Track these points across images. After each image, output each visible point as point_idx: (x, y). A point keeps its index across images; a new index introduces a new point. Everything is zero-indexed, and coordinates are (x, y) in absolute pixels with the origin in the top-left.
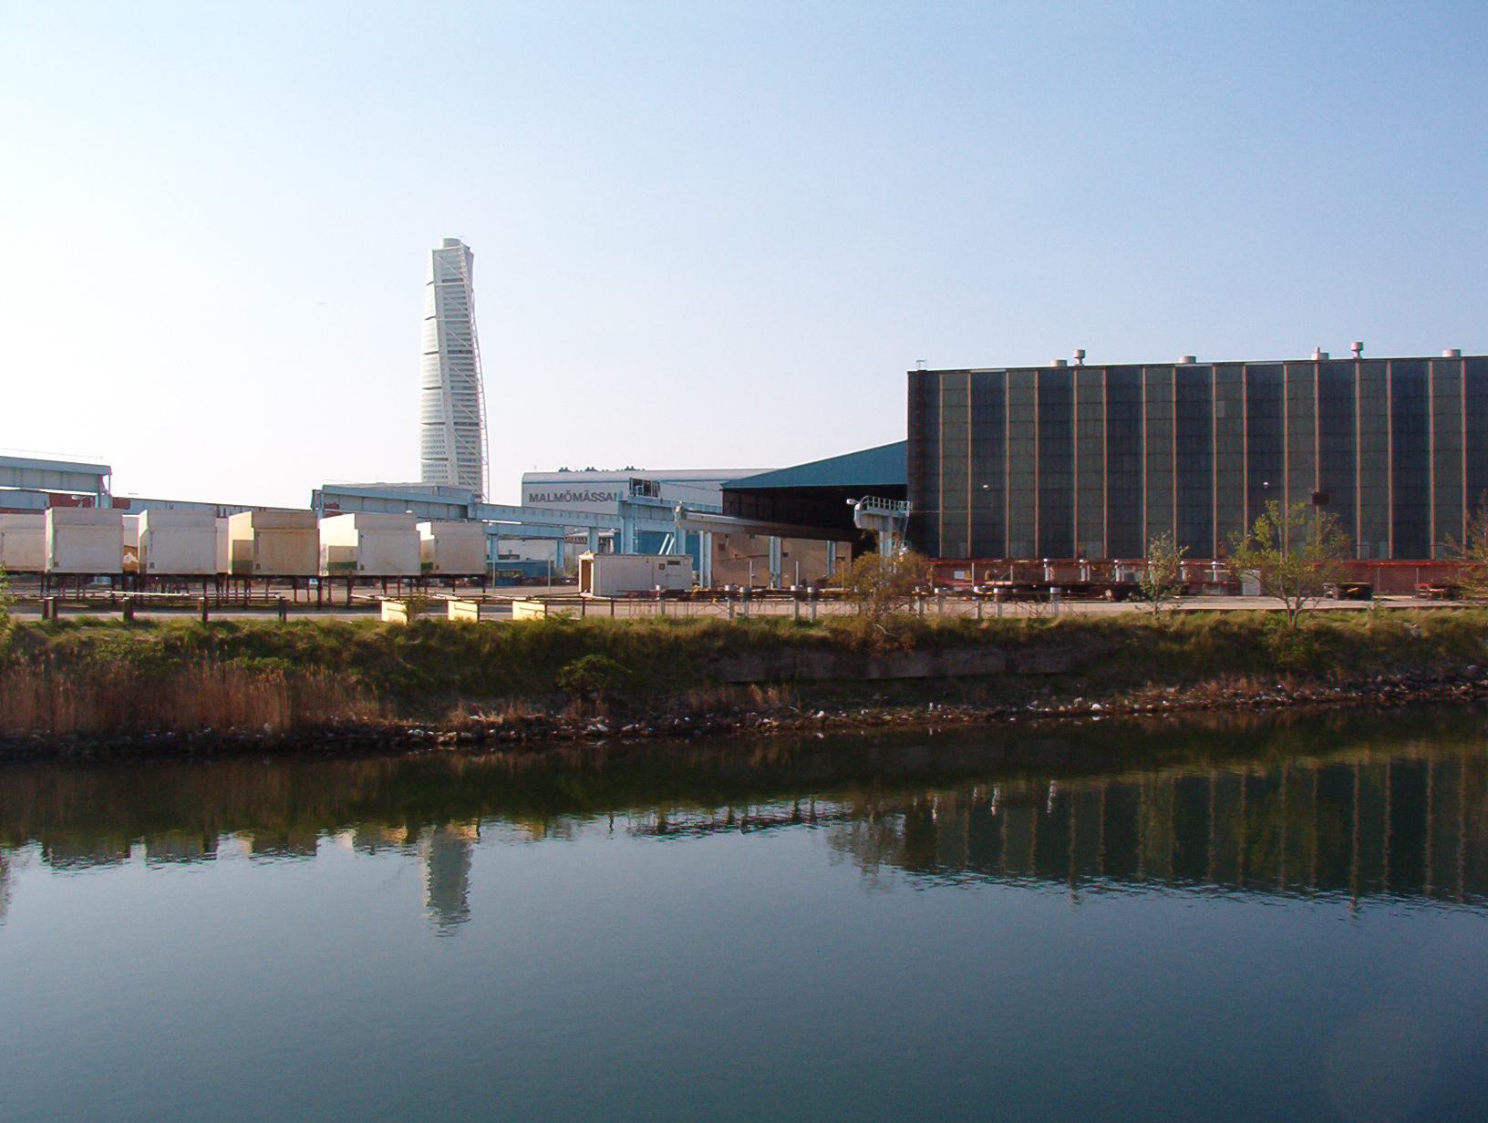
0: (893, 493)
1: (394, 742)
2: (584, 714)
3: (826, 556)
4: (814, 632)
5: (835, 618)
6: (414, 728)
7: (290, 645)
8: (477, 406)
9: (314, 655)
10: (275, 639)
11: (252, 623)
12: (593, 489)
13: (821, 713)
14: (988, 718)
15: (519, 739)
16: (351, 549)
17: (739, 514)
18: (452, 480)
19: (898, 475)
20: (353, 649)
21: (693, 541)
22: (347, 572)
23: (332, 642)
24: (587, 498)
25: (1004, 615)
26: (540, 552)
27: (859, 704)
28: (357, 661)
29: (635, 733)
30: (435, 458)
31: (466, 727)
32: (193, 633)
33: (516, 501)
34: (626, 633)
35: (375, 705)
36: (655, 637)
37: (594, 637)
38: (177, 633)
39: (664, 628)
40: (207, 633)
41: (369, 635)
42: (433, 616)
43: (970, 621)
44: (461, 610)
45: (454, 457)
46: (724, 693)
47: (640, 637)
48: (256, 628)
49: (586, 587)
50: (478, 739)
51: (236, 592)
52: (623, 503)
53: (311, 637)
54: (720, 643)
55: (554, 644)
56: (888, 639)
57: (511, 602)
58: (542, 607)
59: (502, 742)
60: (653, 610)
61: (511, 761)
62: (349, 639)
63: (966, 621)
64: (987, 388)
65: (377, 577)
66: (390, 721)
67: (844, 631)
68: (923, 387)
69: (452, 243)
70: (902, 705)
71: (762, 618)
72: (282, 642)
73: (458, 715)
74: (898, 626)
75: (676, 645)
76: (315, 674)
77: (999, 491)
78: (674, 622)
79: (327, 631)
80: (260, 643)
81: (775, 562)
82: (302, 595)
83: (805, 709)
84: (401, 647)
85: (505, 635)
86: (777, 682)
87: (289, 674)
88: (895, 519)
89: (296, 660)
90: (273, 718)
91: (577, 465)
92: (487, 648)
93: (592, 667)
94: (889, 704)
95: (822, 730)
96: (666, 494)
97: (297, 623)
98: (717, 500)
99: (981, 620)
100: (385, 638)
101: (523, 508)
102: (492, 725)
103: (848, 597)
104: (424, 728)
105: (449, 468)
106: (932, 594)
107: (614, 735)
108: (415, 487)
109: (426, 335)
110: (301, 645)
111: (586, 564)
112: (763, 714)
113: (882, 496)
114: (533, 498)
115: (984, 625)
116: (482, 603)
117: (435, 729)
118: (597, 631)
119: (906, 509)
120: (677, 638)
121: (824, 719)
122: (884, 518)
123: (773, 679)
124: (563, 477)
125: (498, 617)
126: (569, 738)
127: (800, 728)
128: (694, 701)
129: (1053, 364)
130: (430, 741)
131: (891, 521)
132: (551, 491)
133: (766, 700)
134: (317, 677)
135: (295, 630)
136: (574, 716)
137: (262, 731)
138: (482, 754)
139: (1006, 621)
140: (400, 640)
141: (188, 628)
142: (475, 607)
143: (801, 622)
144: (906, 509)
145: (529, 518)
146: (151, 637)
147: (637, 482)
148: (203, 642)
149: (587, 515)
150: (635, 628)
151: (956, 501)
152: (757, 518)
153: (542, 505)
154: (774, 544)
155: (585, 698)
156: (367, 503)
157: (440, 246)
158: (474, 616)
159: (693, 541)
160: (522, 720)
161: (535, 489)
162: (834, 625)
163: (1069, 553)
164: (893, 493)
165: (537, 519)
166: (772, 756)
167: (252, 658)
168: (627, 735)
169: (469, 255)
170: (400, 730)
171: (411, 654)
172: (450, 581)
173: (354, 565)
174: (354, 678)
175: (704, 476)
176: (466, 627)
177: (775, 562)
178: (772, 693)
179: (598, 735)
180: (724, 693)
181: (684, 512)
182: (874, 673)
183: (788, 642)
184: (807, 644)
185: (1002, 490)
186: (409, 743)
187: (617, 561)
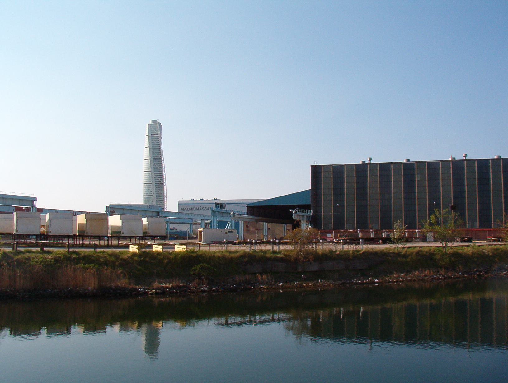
0: (306, 207)
2: (199, 284)
3: (283, 229)
4: (279, 255)
5: (286, 251)
6: (141, 289)
8: (163, 178)
9: (106, 263)
10: (92, 258)
11: (85, 252)
12: (204, 206)
13: (281, 284)
15: (177, 293)
17: (253, 215)
18: (154, 203)
19: (309, 202)
21: (237, 224)
22: (117, 234)
23: (112, 259)
24: (201, 209)
26: (185, 228)
28: (121, 265)
29: (217, 291)
30: (148, 195)
31: (158, 288)
32: (64, 255)
34: (214, 256)
35: (127, 281)
36: (224, 257)
38: (59, 255)
39: (227, 254)
41: (125, 257)
42: (147, 250)
44: (157, 248)
46: (248, 277)
47: (219, 258)
48: (86, 254)
49: (200, 240)
50: (163, 293)
52: (213, 211)
53: (105, 257)
54: (246, 259)
55: (189, 260)
56: (305, 258)
57: (174, 245)
58: (185, 247)
59: (171, 294)
60: (223, 248)
62: (118, 258)
63: (331, 251)
64: (338, 170)
66: (132, 286)
67: (289, 255)
68: (316, 171)
69: (154, 121)
71: (261, 251)
73: (156, 284)
74: (308, 253)
75: (231, 260)
76: (106, 270)
77: (342, 206)
78: (230, 252)
79: (111, 255)
80: (87, 259)
82: (102, 242)
83: (276, 282)
84: (136, 260)
85: (172, 256)
87: (97, 270)
89: (100, 265)
90: (92, 285)
91: (197, 198)
92: (166, 261)
93: (202, 268)
95: (282, 289)
96: (228, 208)
97: (100, 252)
98: (245, 210)
102: (168, 288)
103: (290, 243)
107: (210, 291)
108: (141, 205)
109: (145, 153)
110: (101, 260)
111: (200, 232)
112: (261, 284)
114: (182, 209)
115: (338, 253)
116: (164, 245)
117: (148, 289)
119: (311, 213)
120: (231, 258)
121: (282, 285)
122: (303, 216)
124: (192, 202)
125: (170, 250)
127: (275, 289)
128: (237, 279)
129: (361, 163)
130: (146, 293)
133: (262, 279)
134: (107, 271)
137: (88, 289)
140: (136, 258)
142: (162, 247)
143: (274, 252)
144: (311, 213)
145: (181, 216)
146: (49, 257)
149: (200, 215)
150: (217, 254)
151: (327, 211)
153: (185, 212)
154: (265, 225)
157: (151, 123)
158: (161, 250)
159: (237, 224)
161: (182, 206)
163: (367, 228)
164: (306, 207)
165: (183, 216)
166: (264, 298)
167: (85, 264)
168: (214, 291)
169: (160, 126)
170: (136, 289)
171: (140, 263)
172: (153, 238)
173: (120, 232)
174: (120, 271)
176: (159, 254)
178: (264, 277)
179: (204, 291)
180: (248, 277)
181: (234, 214)
182: (300, 270)
183: (270, 259)
184: (276, 259)
186: (138, 294)
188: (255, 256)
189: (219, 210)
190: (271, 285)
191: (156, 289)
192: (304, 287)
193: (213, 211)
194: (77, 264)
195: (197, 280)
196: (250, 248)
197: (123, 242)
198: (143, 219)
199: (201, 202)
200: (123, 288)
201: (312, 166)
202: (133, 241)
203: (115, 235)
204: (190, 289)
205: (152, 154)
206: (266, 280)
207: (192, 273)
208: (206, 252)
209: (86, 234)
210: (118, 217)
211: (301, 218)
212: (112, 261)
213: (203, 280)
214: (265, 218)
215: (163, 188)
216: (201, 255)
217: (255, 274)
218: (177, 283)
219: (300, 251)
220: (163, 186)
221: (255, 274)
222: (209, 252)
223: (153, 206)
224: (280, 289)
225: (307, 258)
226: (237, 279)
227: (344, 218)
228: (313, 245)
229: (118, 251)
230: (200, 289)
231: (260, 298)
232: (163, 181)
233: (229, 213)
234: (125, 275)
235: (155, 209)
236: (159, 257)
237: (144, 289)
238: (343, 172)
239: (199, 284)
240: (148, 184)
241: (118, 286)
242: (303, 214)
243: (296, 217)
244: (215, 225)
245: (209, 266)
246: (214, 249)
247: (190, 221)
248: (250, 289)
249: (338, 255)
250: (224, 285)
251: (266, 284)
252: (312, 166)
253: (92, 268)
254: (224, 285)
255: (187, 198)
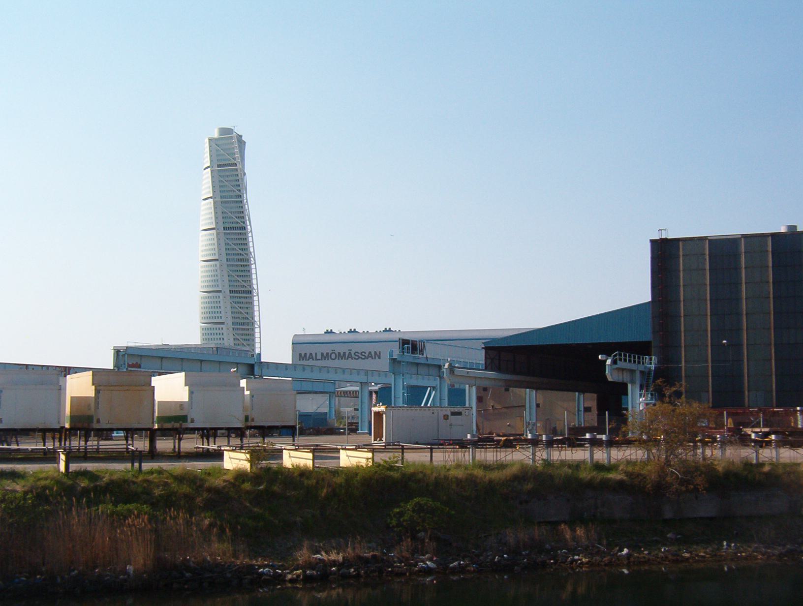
0: (639, 349)
1: (246, 580)
2: (415, 551)
3: (574, 407)
4: (612, 476)
5: (629, 462)
6: (265, 566)
7: (147, 492)
8: (250, 276)
9: (169, 501)
10: (133, 487)
11: (112, 473)
12: (356, 348)
13: (626, 551)
14: (781, 556)
15: (358, 576)
16: (181, 405)
17: (498, 369)
18: (228, 341)
19: (644, 333)
20: (205, 495)
21: (457, 396)
22: (175, 423)
23: (185, 489)
24: (350, 356)
25: (782, 461)
26: (311, 405)
27: (657, 542)
28: (209, 505)
29: (462, 569)
30: (212, 322)
31: (311, 565)
32: (58, 482)
33: (289, 361)
34: (446, 478)
35: (226, 546)
36: (471, 481)
37: (419, 481)
38: (43, 483)
39: (479, 473)
40: (70, 482)
41: (218, 482)
42: (273, 464)
43: (751, 464)
44: (295, 458)
45: (230, 321)
46: (538, 532)
47: (459, 481)
48: (115, 477)
49: (378, 436)
50: (322, 576)
51: (164, 445)
52: (394, 361)
53: (166, 484)
54: (530, 486)
55: (379, 490)
56: (682, 482)
57: (338, 451)
58: (370, 455)
59: (344, 579)
60: (466, 456)
61: (350, 597)
62: (201, 486)
63: (747, 465)
64: (723, 252)
65: (34, 430)
66: (243, 560)
67: (639, 475)
68: (665, 253)
69: (226, 132)
70: (697, 544)
71: (563, 463)
72: (140, 490)
73: (303, 555)
74: (690, 471)
75: (491, 488)
76: (174, 518)
77: (736, 346)
78: (487, 467)
79: (181, 479)
80: (120, 491)
81: (529, 415)
82: (105, 445)
83: (609, 546)
84: (248, 492)
85: (339, 480)
86: (583, 522)
87: (152, 518)
88: (642, 372)
89: (154, 505)
90: (137, 560)
91: (341, 327)
92: (324, 492)
93: (419, 509)
94: (686, 541)
95: (628, 566)
96: (431, 353)
97: (151, 472)
98: (480, 358)
99: (762, 465)
100: (233, 485)
101: (294, 366)
102: (334, 563)
103: (640, 443)
104: (272, 567)
105: (225, 331)
106: (714, 440)
107: (443, 571)
108: (196, 348)
109: (204, 213)
110: (157, 492)
111: (379, 415)
112: (574, 551)
113: (620, 350)
114: (302, 357)
115: (766, 469)
116: (316, 451)
117: (282, 567)
118: (421, 476)
119: (652, 363)
120: (490, 481)
121: (629, 556)
122: (632, 371)
123: (575, 520)
124: (329, 338)
125: (329, 464)
126: (402, 574)
127: (610, 564)
128: (511, 540)
129: (783, 230)
130: (279, 579)
131: (638, 375)
132: (319, 350)
133: (574, 538)
134: (176, 521)
135: (151, 477)
136: (406, 554)
137: (126, 573)
138: (323, 591)
139: (785, 465)
140: (247, 486)
141: (53, 479)
142: (310, 455)
143: (599, 467)
144: (652, 363)
145: (299, 374)
146: (18, 487)
147: (405, 342)
148: (69, 490)
149: (358, 371)
150: (454, 473)
151: (696, 355)
152: (514, 372)
153: (311, 362)
154: (530, 396)
155: (414, 538)
156: (204, 365)
157: (216, 135)
158: (310, 463)
159: (457, 396)
160: (360, 558)
161: (304, 348)
162: (630, 469)
163: (741, 404)
164: (639, 349)
165: (308, 375)
166: (581, 590)
167: (115, 504)
168: (454, 571)
169: (241, 143)
170: (251, 569)
171: (257, 498)
172: (289, 431)
173: (184, 418)
174: (207, 522)
175: (455, 336)
176: (303, 473)
177: (529, 415)
178: (580, 532)
179: (428, 571)
180: (538, 532)
181: (452, 368)
182: (668, 514)
183: (589, 485)
184: (606, 486)
185: (739, 346)
186: (259, 581)
187: (414, 412)
188: (551, 477)
189: (409, 357)
190: (599, 552)
191: (304, 568)
192: (687, 559)
193: (394, 361)
194: (97, 504)
195: (407, 543)
196: (534, 454)
197: (190, 444)
198: (242, 381)
199: (352, 337)
200: (217, 565)
201: (652, 241)
202: (236, 441)
203: (168, 425)
204: (392, 566)
205: (220, 215)
206: (584, 542)
207: (394, 522)
208: (423, 466)
209: (95, 426)
210: (180, 377)
211: (626, 377)
212: (186, 496)
213: (422, 541)
214: (528, 379)
215: (252, 303)
216: (413, 475)
217: (557, 523)
218: (357, 551)
219: (668, 462)
220: (252, 298)
221: (557, 523)
222: (434, 469)
223: (228, 350)
224: (623, 566)
225: (688, 482)
226: (511, 540)
227: (741, 376)
228: (695, 447)
229: (198, 466)
230: (416, 565)
231: (569, 588)
232: (251, 286)
233: (440, 367)
234: (222, 531)
235: (225, 353)
236: (306, 482)
237: (272, 567)
238: (736, 256)
239: (415, 551)
240: (213, 292)
241: (205, 560)
242: (633, 366)
243: (615, 374)
244: (399, 395)
245: (438, 504)
246: (442, 458)
247: (329, 388)
248: (544, 565)
249: (767, 474)
250: (478, 556)
251: (586, 551)
252: (652, 241)
253: (139, 517)
254: (478, 556)
255: (315, 328)
